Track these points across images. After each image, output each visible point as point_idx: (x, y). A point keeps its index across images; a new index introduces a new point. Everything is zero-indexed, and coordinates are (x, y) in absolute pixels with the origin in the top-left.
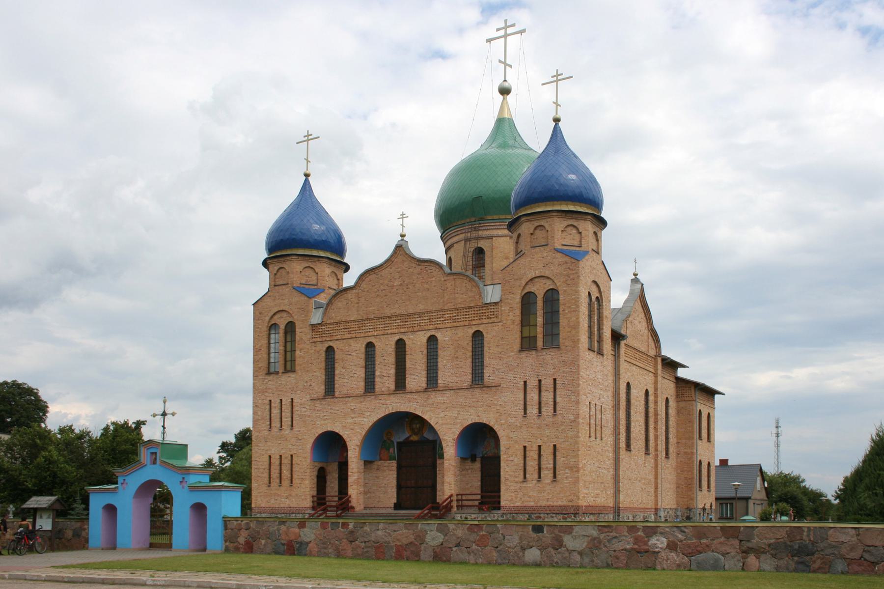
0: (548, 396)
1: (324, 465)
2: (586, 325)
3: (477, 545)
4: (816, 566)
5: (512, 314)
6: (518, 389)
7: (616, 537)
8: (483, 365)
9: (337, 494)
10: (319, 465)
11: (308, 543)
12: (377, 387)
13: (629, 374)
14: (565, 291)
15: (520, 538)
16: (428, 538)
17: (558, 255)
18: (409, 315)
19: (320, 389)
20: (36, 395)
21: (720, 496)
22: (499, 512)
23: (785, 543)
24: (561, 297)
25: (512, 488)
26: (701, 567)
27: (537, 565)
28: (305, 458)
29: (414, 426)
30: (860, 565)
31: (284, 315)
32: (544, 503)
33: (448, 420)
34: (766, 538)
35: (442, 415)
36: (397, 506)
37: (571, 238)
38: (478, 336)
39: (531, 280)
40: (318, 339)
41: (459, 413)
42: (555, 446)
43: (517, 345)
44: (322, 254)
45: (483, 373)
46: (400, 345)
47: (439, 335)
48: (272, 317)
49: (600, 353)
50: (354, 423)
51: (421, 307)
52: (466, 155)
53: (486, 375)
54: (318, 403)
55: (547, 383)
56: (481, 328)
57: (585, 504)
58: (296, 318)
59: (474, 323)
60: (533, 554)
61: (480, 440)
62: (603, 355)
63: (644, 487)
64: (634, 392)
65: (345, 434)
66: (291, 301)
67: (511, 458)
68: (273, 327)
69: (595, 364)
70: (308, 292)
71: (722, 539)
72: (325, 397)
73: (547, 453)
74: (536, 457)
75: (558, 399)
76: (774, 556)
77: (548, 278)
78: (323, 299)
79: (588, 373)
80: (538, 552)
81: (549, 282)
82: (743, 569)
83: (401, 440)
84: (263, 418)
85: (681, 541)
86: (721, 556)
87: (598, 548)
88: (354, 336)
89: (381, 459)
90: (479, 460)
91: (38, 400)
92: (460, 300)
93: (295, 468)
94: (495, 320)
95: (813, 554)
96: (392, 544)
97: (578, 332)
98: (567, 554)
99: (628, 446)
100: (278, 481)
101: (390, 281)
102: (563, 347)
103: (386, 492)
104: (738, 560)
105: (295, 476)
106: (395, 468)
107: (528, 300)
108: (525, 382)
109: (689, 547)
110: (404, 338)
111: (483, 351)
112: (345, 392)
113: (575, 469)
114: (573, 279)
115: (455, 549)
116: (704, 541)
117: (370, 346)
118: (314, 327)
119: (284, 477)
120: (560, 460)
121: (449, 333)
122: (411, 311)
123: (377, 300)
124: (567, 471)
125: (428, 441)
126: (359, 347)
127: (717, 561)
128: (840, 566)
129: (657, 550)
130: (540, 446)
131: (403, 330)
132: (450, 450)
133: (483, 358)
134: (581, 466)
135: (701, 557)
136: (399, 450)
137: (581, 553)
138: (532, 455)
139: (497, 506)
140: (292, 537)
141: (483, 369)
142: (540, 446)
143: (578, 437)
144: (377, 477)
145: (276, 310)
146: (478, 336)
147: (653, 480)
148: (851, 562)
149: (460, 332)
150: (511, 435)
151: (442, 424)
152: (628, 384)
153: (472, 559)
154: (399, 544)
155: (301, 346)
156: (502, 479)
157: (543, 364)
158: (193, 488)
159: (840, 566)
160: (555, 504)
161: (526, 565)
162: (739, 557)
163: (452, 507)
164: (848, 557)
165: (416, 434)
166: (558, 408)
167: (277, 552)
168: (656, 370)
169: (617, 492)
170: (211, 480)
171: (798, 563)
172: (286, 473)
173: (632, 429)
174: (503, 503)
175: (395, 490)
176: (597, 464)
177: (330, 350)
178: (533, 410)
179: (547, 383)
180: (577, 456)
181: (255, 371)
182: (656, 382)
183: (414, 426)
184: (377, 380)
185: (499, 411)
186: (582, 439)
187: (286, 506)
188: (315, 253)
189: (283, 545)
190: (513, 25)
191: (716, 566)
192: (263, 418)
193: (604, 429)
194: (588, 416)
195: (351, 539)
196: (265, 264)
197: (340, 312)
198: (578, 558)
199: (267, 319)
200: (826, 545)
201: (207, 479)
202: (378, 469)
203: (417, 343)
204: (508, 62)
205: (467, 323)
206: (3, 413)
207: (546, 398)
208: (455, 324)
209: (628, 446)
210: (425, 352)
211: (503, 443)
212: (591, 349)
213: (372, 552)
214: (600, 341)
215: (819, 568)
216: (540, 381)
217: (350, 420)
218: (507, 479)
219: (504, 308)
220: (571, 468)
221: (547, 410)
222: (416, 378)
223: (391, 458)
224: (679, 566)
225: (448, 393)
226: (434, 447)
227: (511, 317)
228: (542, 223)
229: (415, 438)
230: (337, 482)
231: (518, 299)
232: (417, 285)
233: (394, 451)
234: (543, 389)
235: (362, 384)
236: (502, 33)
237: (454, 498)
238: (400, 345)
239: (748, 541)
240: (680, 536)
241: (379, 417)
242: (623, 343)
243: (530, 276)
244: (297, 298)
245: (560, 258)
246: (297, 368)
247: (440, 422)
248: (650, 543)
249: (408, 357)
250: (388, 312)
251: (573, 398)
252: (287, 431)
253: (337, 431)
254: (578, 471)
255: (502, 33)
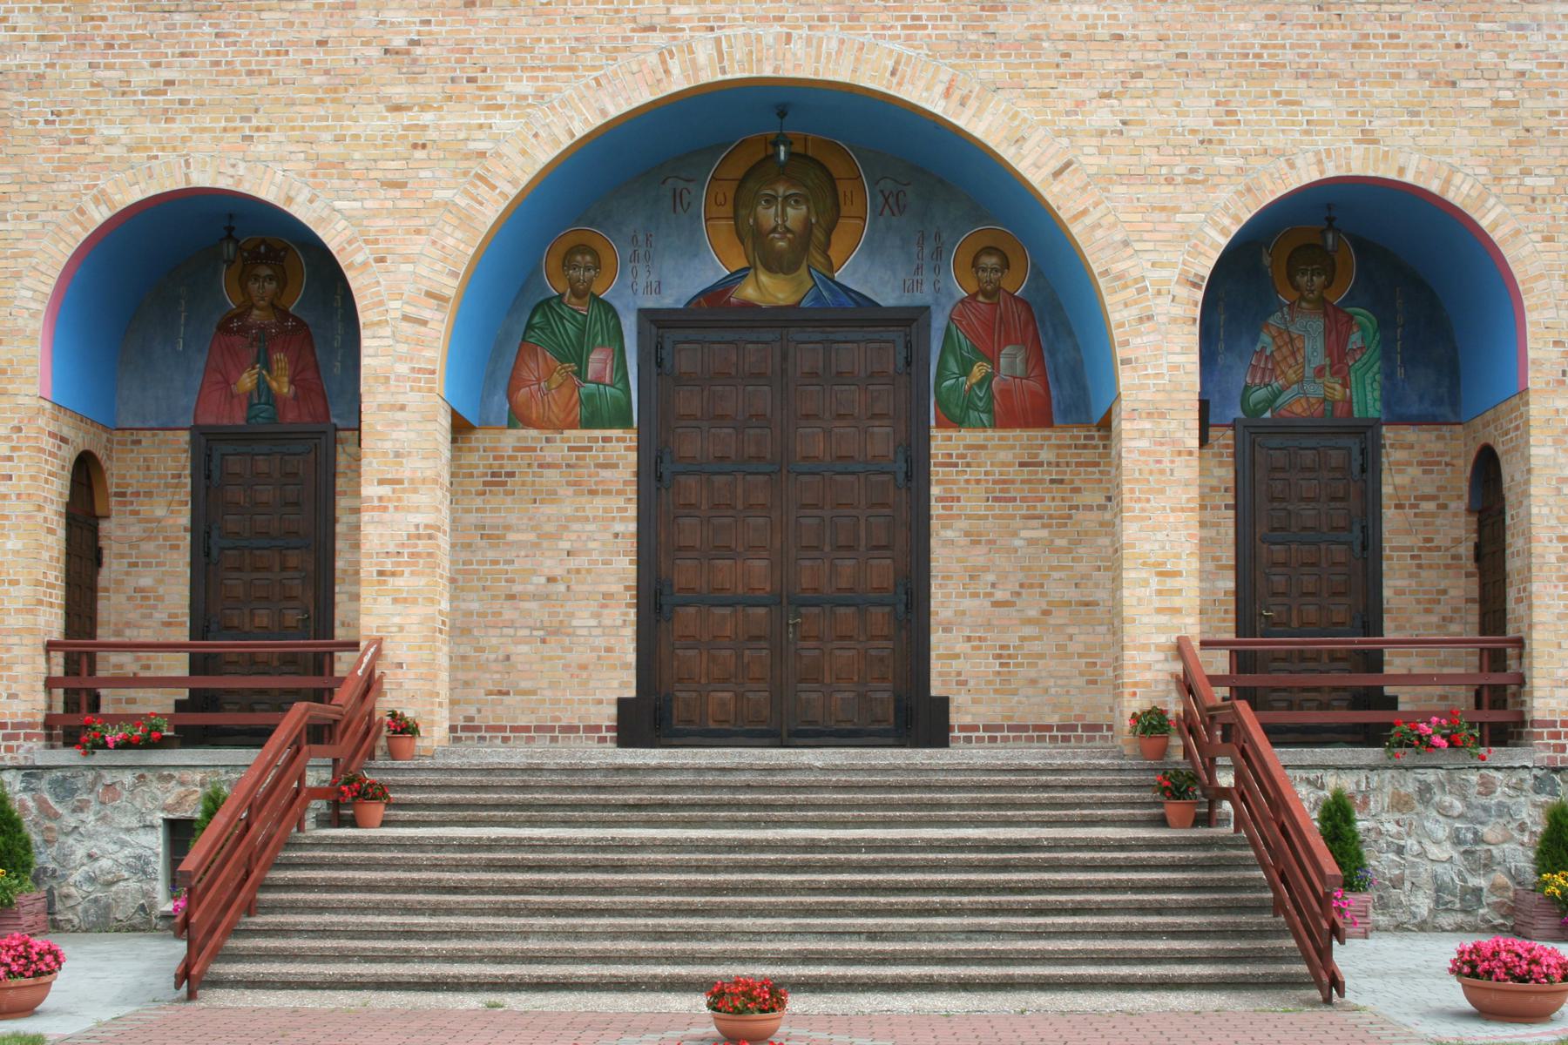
9: (182, 635)
10: (81, 440)
21: (1209, 637)
29: (768, 216)
35: (1103, 116)
36: (641, 721)
41: (1227, 114)
89: (517, 418)
103: (555, 631)
125: (863, 315)
132: (1155, 357)
136: (655, 359)
151: (1107, 179)
165: (777, 264)
183: (768, 216)
206: (7, 776)
217: (373, 122)
229: (769, 289)
230: (180, 563)
233: (618, 366)
241: (616, 108)
247: (1090, 161)
253: (268, 192)
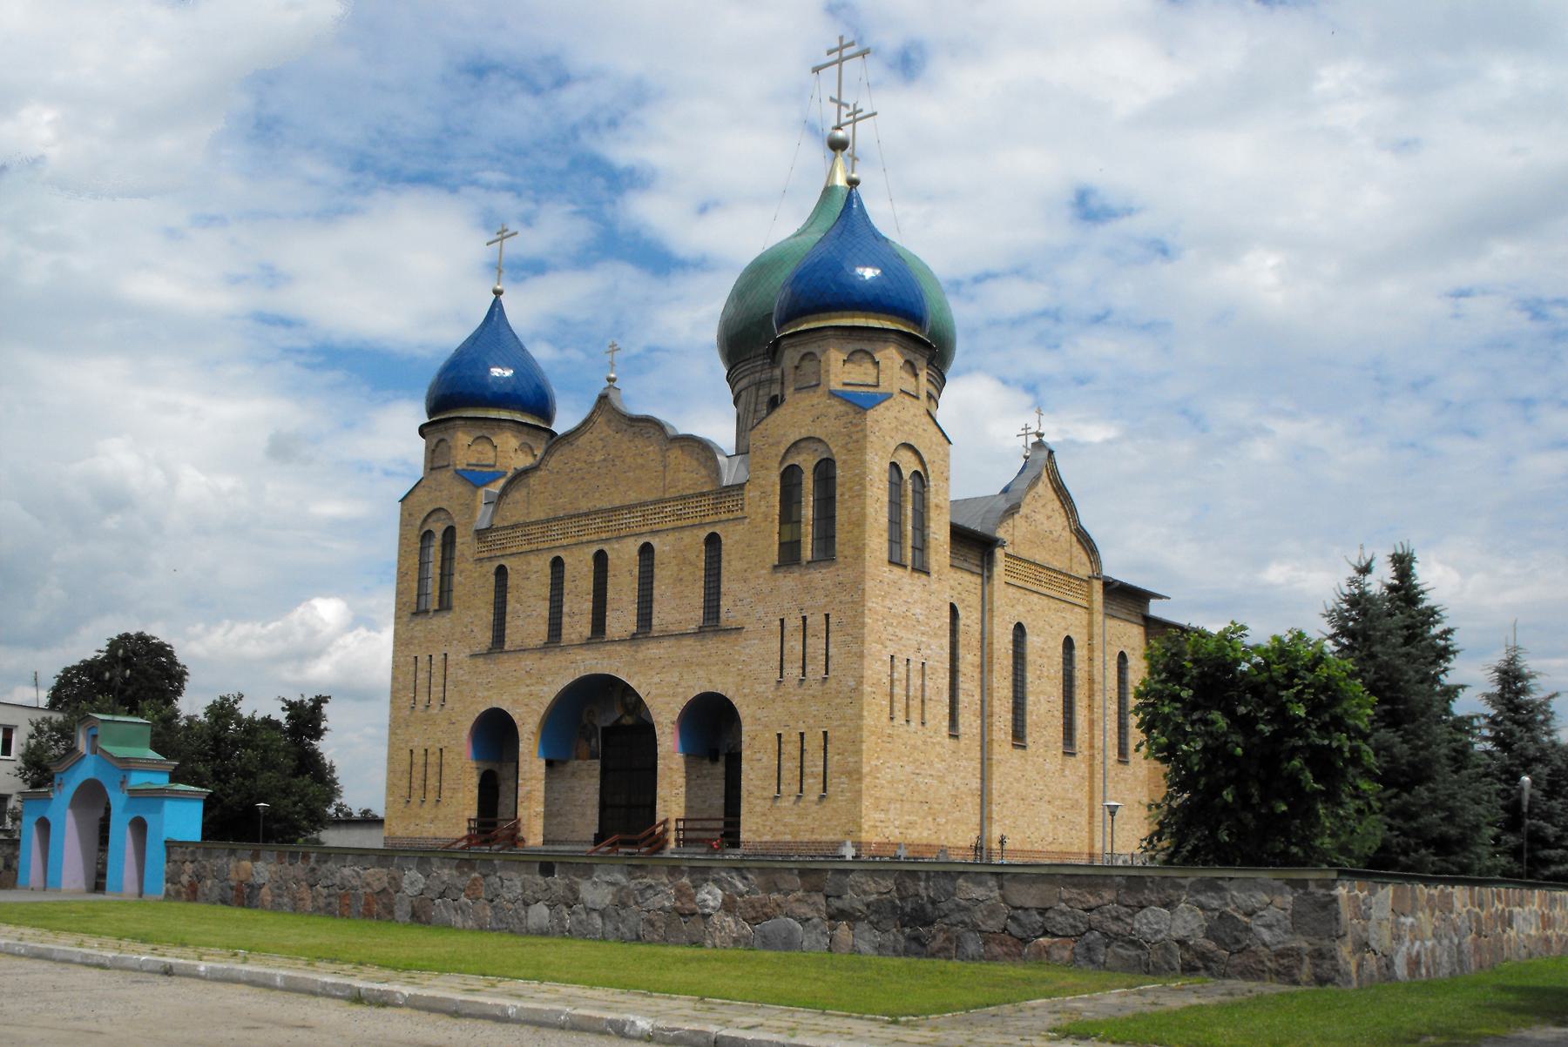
0: (816, 645)
1: (495, 767)
2: (884, 519)
3: (467, 896)
4: (936, 945)
5: (765, 502)
6: (771, 632)
7: (650, 887)
8: (719, 593)
11: (261, 886)
12: (564, 631)
13: (1020, 608)
14: (845, 462)
15: (523, 887)
16: (405, 883)
17: (834, 402)
18: (614, 509)
19: (485, 637)
20: (170, 654)
22: (738, 851)
23: (892, 902)
24: (838, 472)
25: (758, 809)
26: (767, 943)
27: (543, 933)
28: (459, 754)
30: (1001, 944)
31: (442, 515)
32: (806, 837)
33: (664, 687)
34: (865, 892)
35: (656, 679)
37: (860, 373)
38: (713, 542)
39: (795, 444)
40: (486, 555)
42: (825, 733)
43: (774, 557)
44: (504, 415)
45: (719, 606)
46: (601, 559)
47: (655, 542)
48: (425, 520)
49: (922, 569)
50: (529, 694)
51: (632, 497)
52: (927, 262)
53: (723, 609)
54: (480, 661)
55: (816, 621)
56: (717, 530)
57: (877, 839)
58: (458, 521)
59: (707, 520)
60: (540, 914)
61: (712, 723)
62: (928, 574)
63: (1060, 814)
64: (1033, 641)
65: (516, 714)
66: (450, 493)
67: (758, 756)
68: (427, 536)
69: (907, 588)
70: (475, 478)
71: (800, 894)
72: (490, 652)
73: (814, 744)
74: (797, 753)
75: (832, 651)
76: (875, 925)
77: (820, 441)
78: (496, 488)
79: (888, 603)
80: (546, 911)
81: (821, 448)
82: (830, 950)
83: (607, 724)
84: (405, 688)
85: (741, 895)
86: (798, 926)
87: (625, 906)
88: (534, 547)
89: (577, 758)
90: (722, 759)
91: (173, 662)
92: (688, 482)
93: (446, 771)
94: (739, 514)
95: (932, 923)
96: (361, 891)
97: (864, 532)
98: (584, 916)
99: (1019, 735)
100: (421, 792)
101: (590, 454)
102: (841, 559)
103: (583, 815)
104: (824, 933)
105: (444, 785)
106: (597, 772)
107: (790, 476)
108: (782, 621)
109: (753, 907)
110: (606, 547)
111: (719, 568)
112: (519, 642)
113: (855, 774)
114: (857, 444)
115: (438, 901)
116: (775, 896)
117: (557, 564)
118: (480, 534)
119: (429, 787)
120: (834, 759)
121: (671, 538)
122: (617, 503)
123: (570, 486)
124: (844, 779)
126: (542, 564)
127: (791, 932)
128: (973, 945)
129: (707, 911)
130: (802, 734)
131: (604, 536)
133: (719, 580)
134: (866, 769)
135: (768, 925)
137: (603, 914)
138: (791, 749)
139: (736, 844)
140: (243, 877)
141: (719, 600)
142: (802, 734)
143: (861, 717)
144: (572, 789)
145: (429, 509)
146: (713, 542)
147: (1086, 802)
148: (987, 937)
149: (687, 537)
150: (759, 714)
152: (1019, 630)
153: (458, 920)
154: (368, 890)
155: (462, 566)
156: (744, 793)
157: (815, 586)
158: (135, 794)
159: (973, 945)
160: (824, 838)
161: (528, 932)
162: (825, 926)
163: (667, 841)
164: (984, 927)
166: (831, 667)
167: (224, 902)
168: (1091, 602)
169: (985, 819)
170: (171, 781)
171: (911, 939)
172: (433, 782)
173: (1029, 708)
174: (744, 836)
175: (596, 811)
176: (909, 769)
177: (501, 572)
178: (793, 671)
179: (816, 621)
180: (859, 752)
181: (398, 609)
182: (1091, 624)
184: (565, 619)
185: (739, 671)
186: (869, 721)
187: (431, 835)
188: (493, 414)
189: (232, 888)
190: (852, 44)
191: (789, 943)
192: (405, 688)
193: (929, 705)
194: (886, 680)
195: (312, 881)
196: (423, 431)
197: (515, 510)
198: (598, 921)
199: (419, 522)
200: (951, 906)
201: (166, 778)
202: (573, 774)
203: (624, 556)
204: (844, 100)
205: (697, 521)
207: (822, 649)
208: (679, 523)
209: (1019, 735)
210: (636, 572)
211: (747, 728)
212: (895, 562)
213: (231, 894)
214: (921, 547)
215: (941, 950)
216: (804, 618)
217: (524, 690)
218: (750, 793)
219: (751, 493)
220: (849, 774)
221: (816, 669)
222: (622, 619)
223: (593, 756)
224: (736, 941)
225: (666, 643)
226: (645, 731)
227: (763, 509)
228: (813, 348)
229: (628, 720)
231: (775, 478)
232: (628, 460)
233: (596, 743)
234: (809, 632)
235: (544, 629)
236: (835, 56)
237: (672, 826)
238: (601, 559)
239: (839, 897)
240: (740, 886)
242: (999, 553)
243: (793, 438)
244: (459, 488)
245: (840, 408)
246: (455, 603)
247: (654, 692)
248: (699, 897)
249: (610, 581)
250: (584, 505)
251: (855, 648)
252: (435, 710)
254: (860, 780)
255: (835, 56)
